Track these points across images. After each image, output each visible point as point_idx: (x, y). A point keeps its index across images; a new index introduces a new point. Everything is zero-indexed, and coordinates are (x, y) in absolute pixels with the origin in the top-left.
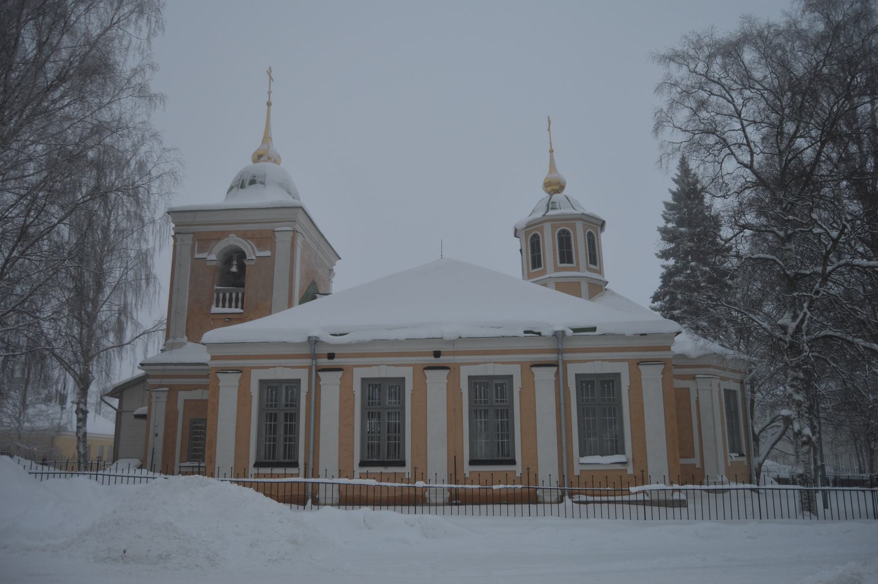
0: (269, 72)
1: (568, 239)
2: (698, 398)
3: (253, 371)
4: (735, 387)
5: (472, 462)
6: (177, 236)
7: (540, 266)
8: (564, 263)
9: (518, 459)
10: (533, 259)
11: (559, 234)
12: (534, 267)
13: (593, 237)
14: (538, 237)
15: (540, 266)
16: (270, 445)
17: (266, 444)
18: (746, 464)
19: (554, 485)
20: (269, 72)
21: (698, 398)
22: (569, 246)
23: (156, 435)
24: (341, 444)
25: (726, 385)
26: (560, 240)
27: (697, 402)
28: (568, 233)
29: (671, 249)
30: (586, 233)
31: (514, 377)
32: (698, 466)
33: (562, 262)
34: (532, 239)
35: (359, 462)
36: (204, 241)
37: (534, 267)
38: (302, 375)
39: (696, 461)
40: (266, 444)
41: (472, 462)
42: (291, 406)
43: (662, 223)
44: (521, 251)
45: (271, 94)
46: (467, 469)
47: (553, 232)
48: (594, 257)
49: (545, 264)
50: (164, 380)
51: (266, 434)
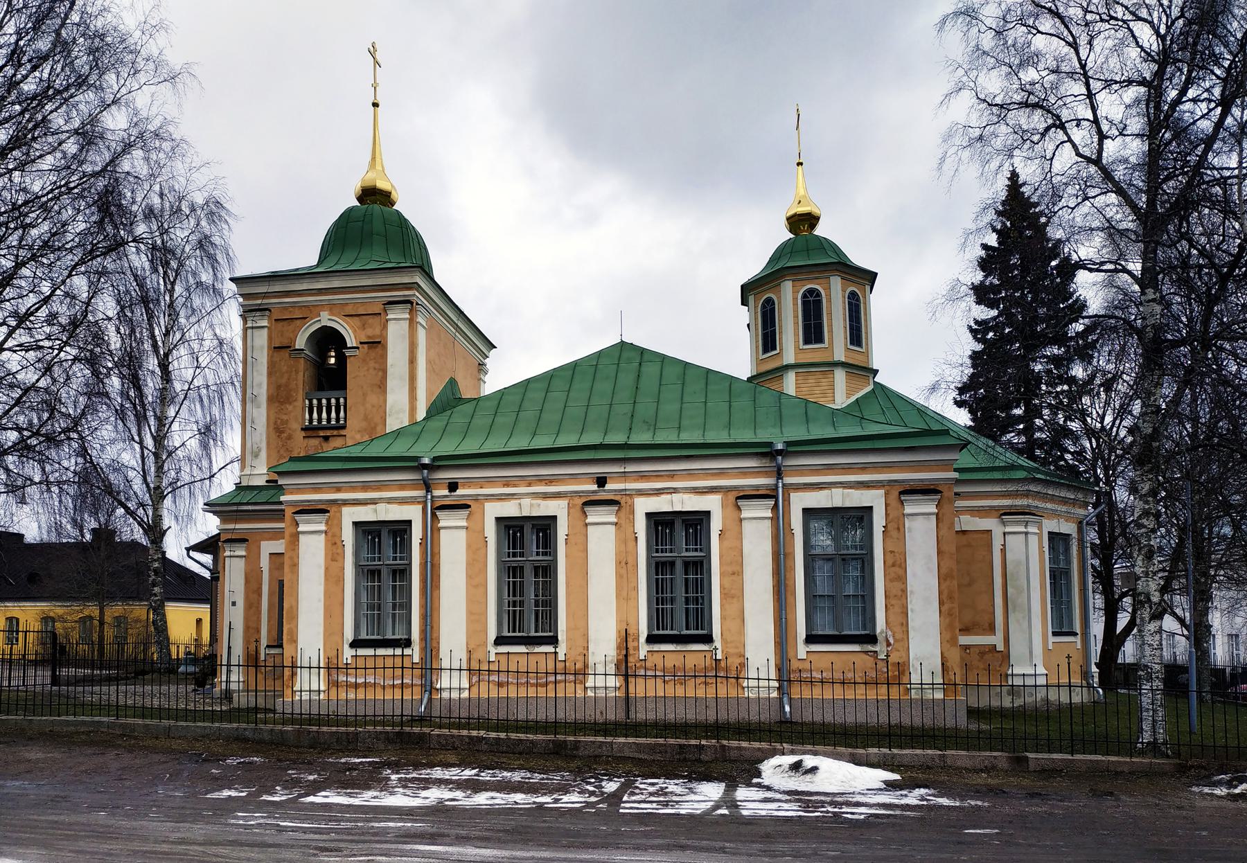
0: (372, 52)
1: (819, 303)
2: (1004, 545)
3: (346, 510)
4: (1068, 528)
5: (810, 639)
6: (247, 315)
7: (820, 339)
8: (323, 390)
9: (562, 636)
10: (765, 337)
11: (804, 296)
12: (765, 351)
13: (858, 300)
14: (773, 303)
15: (820, 339)
16: (662, 605)
17: (509, 611)
18: (1079, 646)
19: (773, 675)
20: (372, 52)
21: (1004, 545)
22: (819, 315)
23: (234, 604)
24: (470, 613)
25: (1051, 525)
26: (805, 304)
27: (1003, 551)
28: (819, 294)
29: (994, 318)
30: (847, 296)
31: (875, 510)
32: (1000, 647)
33: (807, 342)
34: (763, 306)
35: (804, 636)
36: (286, 321)
37: (765, 351)
38: (413, 513)
39: (997, 640)
40: (509, 611)
41: (810, 639)
42: (662, 552)
43: (978, 276)
44: (748, 325)
45: (377, 88)
46: (348, 653)
47: (795, 292)
48: (857, 334)
49: (781, 344)
50: (1001, 477)
51: (509, 596)
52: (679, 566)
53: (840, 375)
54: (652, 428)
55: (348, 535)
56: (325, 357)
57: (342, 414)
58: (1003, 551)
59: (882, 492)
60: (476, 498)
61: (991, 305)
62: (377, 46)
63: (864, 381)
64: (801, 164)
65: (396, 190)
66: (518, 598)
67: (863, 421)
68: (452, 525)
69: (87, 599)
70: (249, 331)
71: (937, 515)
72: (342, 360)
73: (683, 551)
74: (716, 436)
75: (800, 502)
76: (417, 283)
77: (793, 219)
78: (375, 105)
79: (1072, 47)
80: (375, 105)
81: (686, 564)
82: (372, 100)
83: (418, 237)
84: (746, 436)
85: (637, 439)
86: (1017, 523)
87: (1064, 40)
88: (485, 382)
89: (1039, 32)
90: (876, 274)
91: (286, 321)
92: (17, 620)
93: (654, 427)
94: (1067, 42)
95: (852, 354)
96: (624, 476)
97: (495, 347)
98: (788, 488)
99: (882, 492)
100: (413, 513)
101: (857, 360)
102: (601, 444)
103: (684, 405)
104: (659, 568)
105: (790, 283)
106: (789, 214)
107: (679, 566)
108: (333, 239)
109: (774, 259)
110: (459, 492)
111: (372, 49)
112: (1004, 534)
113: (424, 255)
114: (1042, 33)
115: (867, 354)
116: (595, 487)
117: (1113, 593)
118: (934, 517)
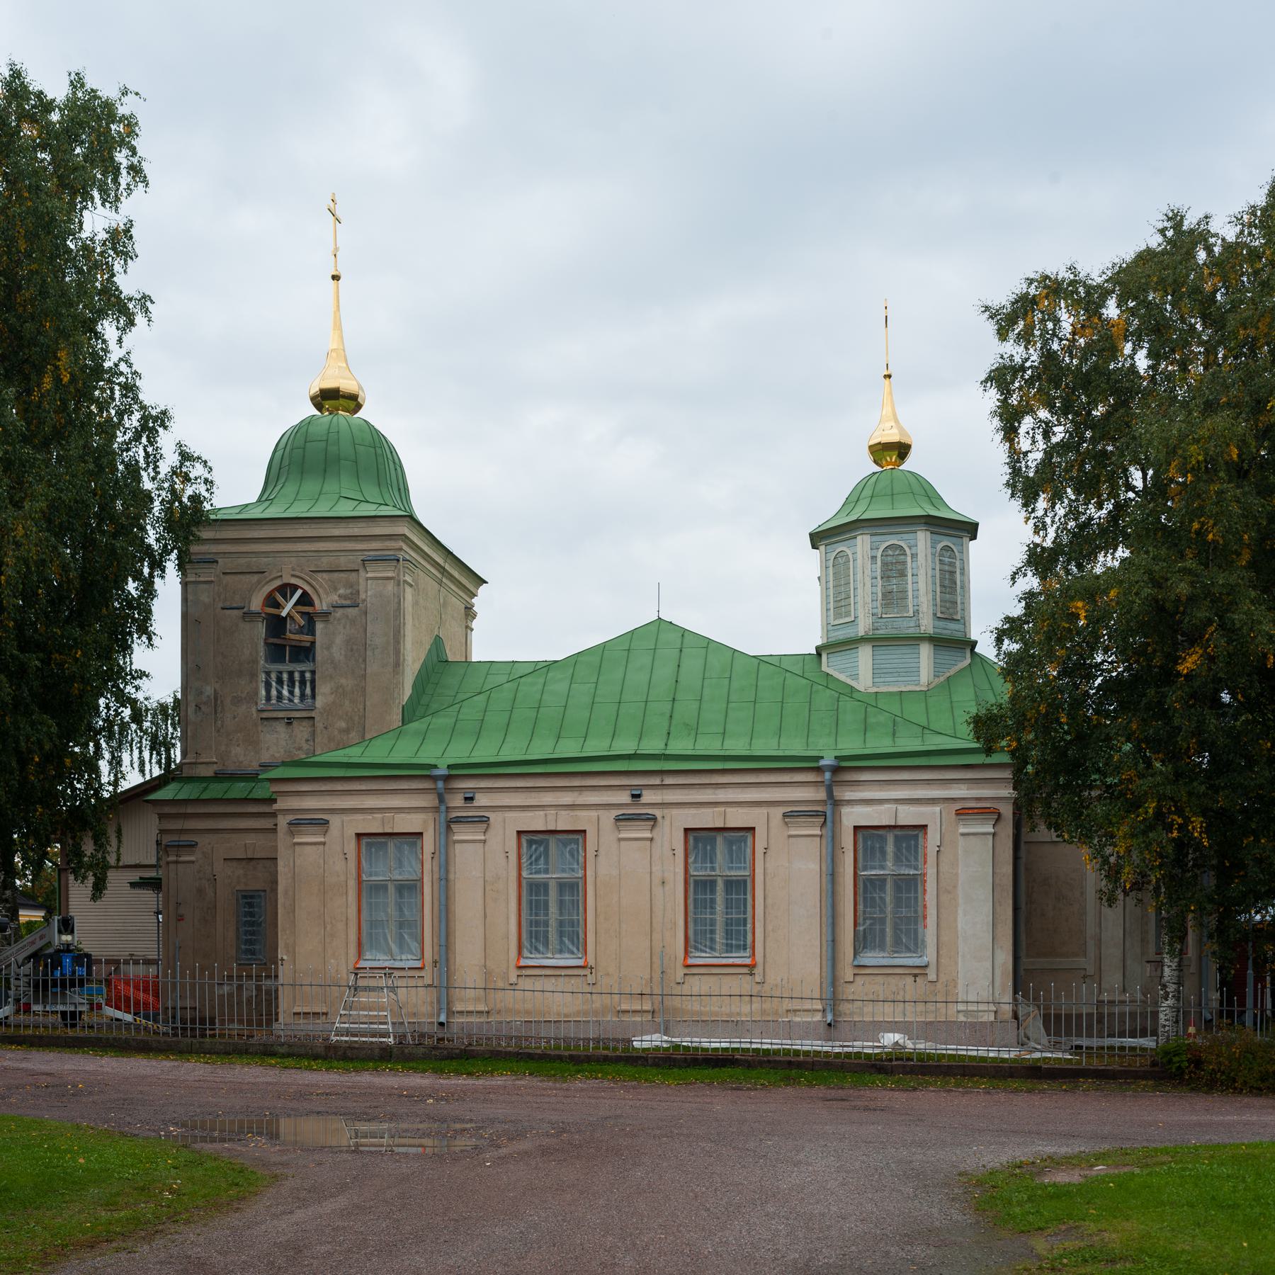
44: (819, 578)
52: (391, 889)
53: (925, 651)
54: (693, 733)
57: (308, 691)
62: (337, 199)
63: (959, 655)
64: (889, 376)
65: (363, 391)
67: (926, 731)
70: (190, 588)
71: (994, 835)
73: (722, 868)
74: (765, 746)
75: (853, 816)
76: (404, 535)
77: (875, 448)
80: (336, 278)
81: (562, 886)
83: (392, 450)
84: (795, 747)
85: (678, 747)
88: (472, 630)
90: (977, 525)
93: (695, 730)
95: (942, 624)
97: (486, 582)
101: (951, 629)
102: (635, 754)
103: (731, 705)
104: (867, 888)
105: (867, 538)
106: (872, 443)
107: (391, 889)
108: (286, 462)
109: (853, 500)
115: (964, 622)
118: (991, 837)
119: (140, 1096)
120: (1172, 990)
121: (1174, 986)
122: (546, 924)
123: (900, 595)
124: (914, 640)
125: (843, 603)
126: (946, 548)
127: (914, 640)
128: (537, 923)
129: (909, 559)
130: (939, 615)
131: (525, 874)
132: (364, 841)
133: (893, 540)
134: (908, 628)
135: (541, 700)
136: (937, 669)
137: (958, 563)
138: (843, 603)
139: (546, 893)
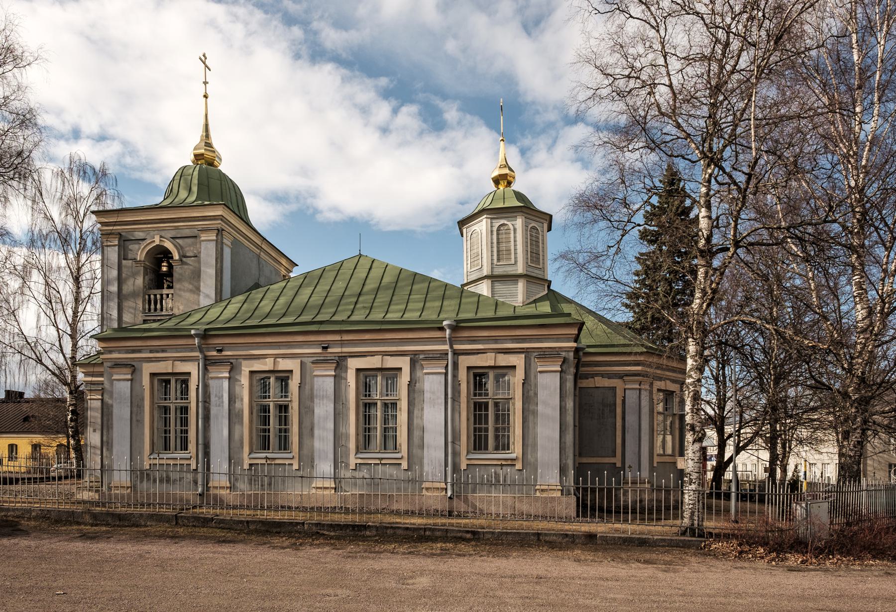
0: (203, 60)
2: (624, 397)
20: (203, 60)
27: (624, 401)
32: (619, 465)
53: (521, 285)
55: (146, 381)
56: (160, 267)
58: (624, 401)
59: (523, 356)
60: (237, 357)
61: (651, 242)
66: (283, 427)
68: (220, 376)
69: (58, 432)
72: (170, 267)
78: (206, 97)
79: (655, 29)
82: (203, 94)
86: (634, 382)
87: (649, 24)
89: (631, 17)
90: (458, 222)
91: (124, 242)
92: (16, 446)
94: (651, 26)
95: (531, 270)
96: (342, 343)
98: (456, 353)
99: (523, 356)
100: (193, 369)
101: (537, 273)
110: (224, 353)
111: (203, 58)
112: (625, 389)
113: (240, 201)
114: (634, 18)
115: (543, 269)
116: (320, 351)
117: (723, 436)
119: (332, 542)
120: (694, 477)
121: (696, 474)
122: (487, 430)
123: (508, 252)
124: (514, 278)
125: (475, 259)
126: (533, 228)
127: (514, 278)
128: (480, 430)
129: (512, 232)
130: (529, 264)
131: (156, 401)
132: (361, 374)
133: (502, 222)
134: (510, 270)
135: (393, 295)
136: (528, 293)
137: (540, 237)
138: (475, 259)
139: (487, 409)
